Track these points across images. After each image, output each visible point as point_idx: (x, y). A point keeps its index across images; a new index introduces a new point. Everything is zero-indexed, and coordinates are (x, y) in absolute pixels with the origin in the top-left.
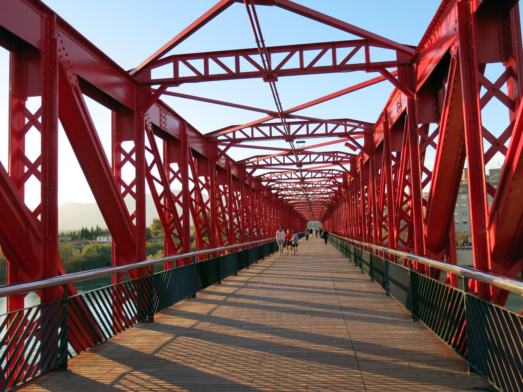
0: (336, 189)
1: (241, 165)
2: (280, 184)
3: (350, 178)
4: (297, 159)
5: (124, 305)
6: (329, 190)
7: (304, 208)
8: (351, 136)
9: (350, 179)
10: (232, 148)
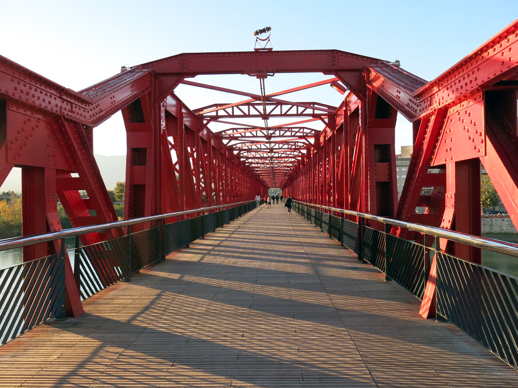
0: (300, 158)
1: (219, 136)
3: (313, 151)
4: (265, 110)
9: (313, 151)
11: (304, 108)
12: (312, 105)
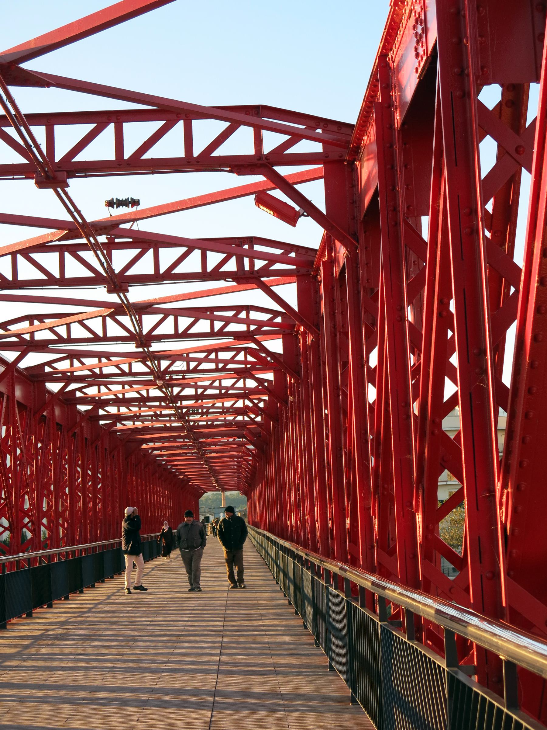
0: (270, 376)
2: (75, 361)
6: (251, 384)
7: (180, 447)
8: (283, 171)
11: (227, 124)
12: (246, 247)
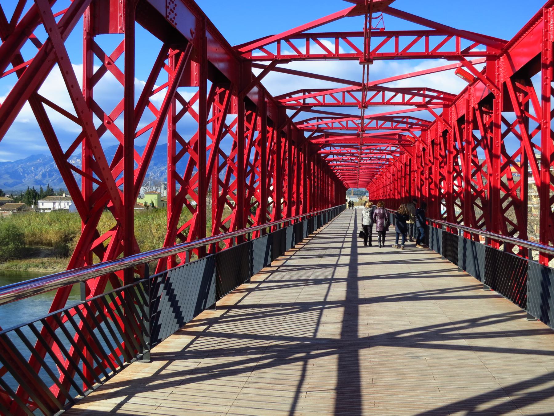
0: (398, 155)
4: (367, 45)
5: (96, 331)
10: (272, 74)
